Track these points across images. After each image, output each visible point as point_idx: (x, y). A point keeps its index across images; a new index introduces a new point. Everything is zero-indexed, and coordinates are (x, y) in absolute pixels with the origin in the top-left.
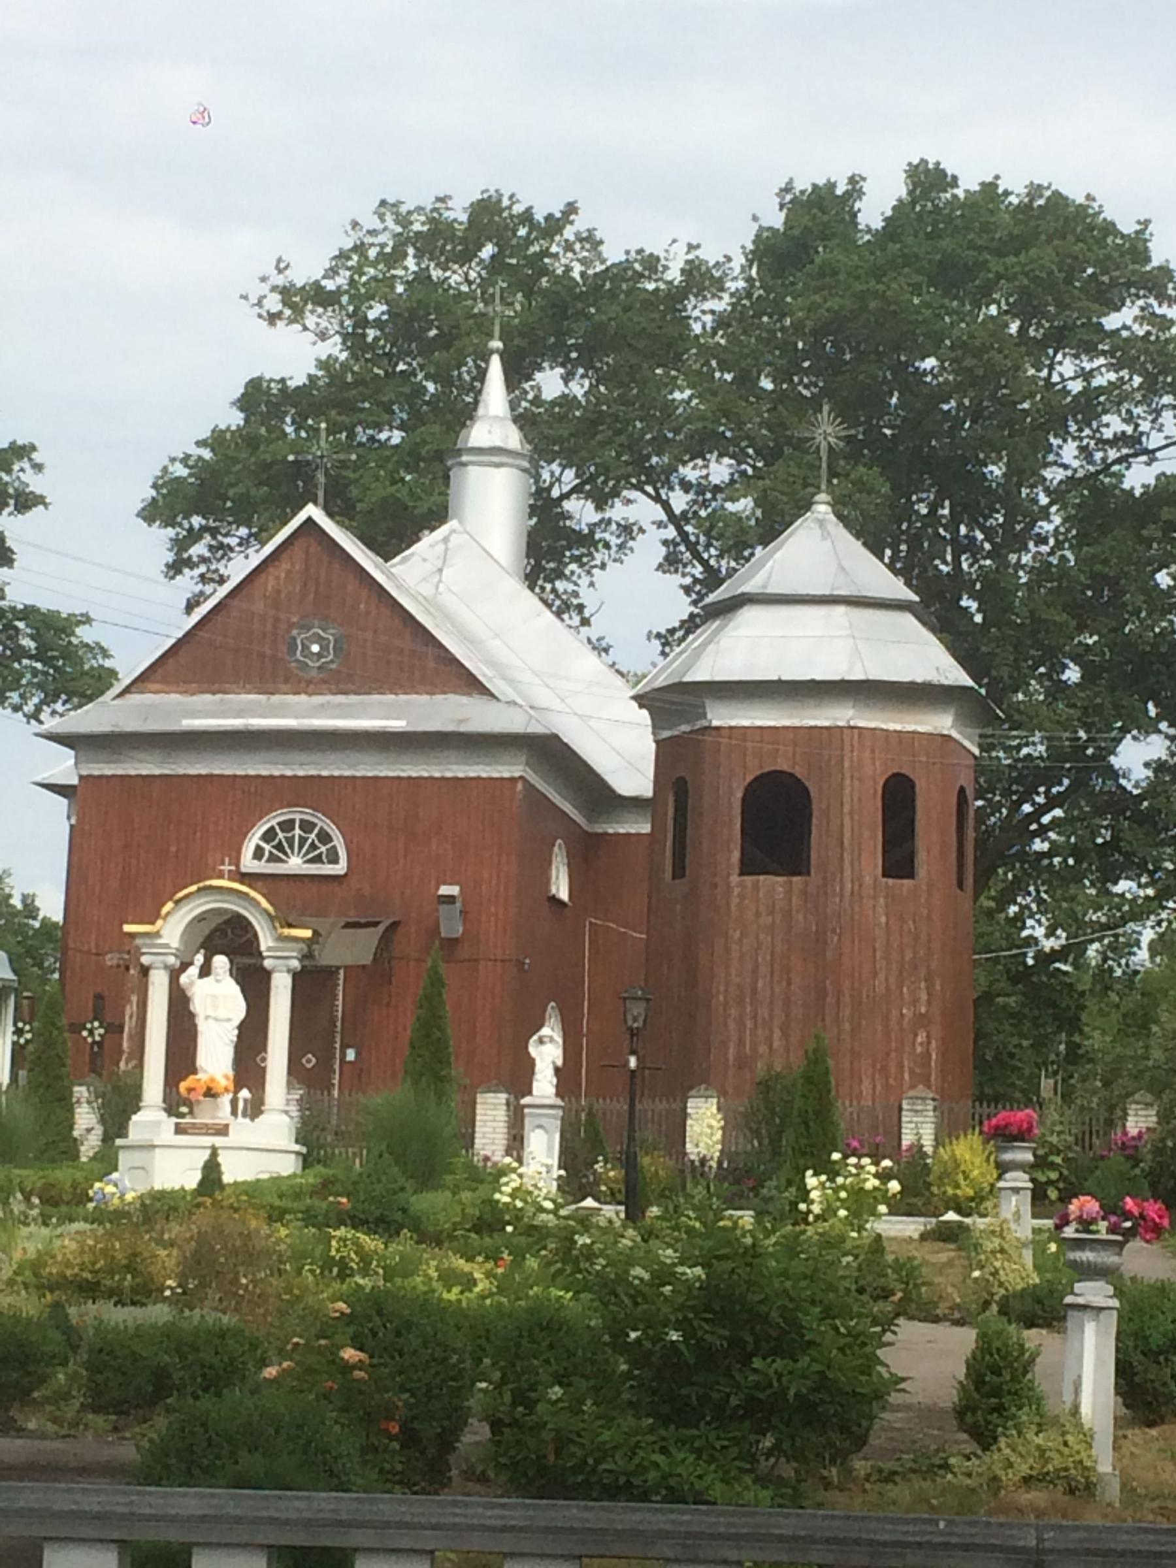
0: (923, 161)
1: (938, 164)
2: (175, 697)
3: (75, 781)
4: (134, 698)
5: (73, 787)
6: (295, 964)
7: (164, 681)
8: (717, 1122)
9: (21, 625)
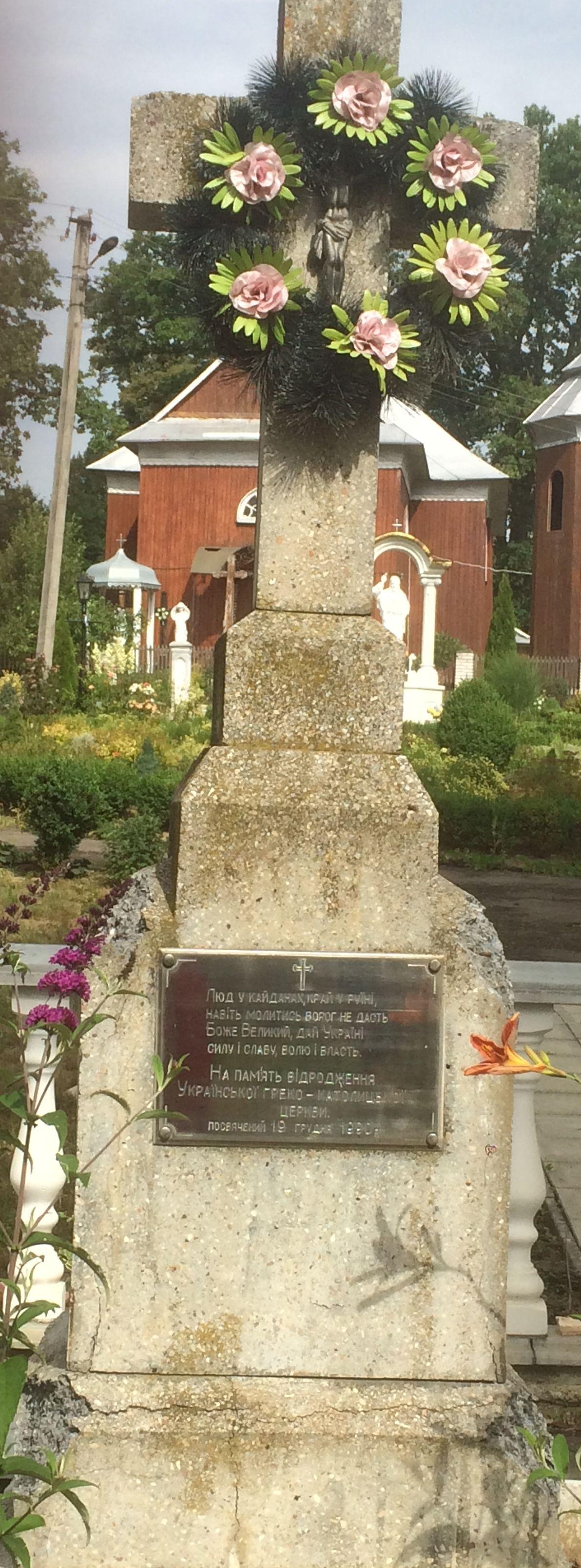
0: (534, 106)
1: (545, 108)
2: (194, 420)
3: (138, 468)
4: (170, 420)
5: (136, 474)
6: (439, 581)
7: (188, 410)
8: (470, 665)
9: (48, 376)
